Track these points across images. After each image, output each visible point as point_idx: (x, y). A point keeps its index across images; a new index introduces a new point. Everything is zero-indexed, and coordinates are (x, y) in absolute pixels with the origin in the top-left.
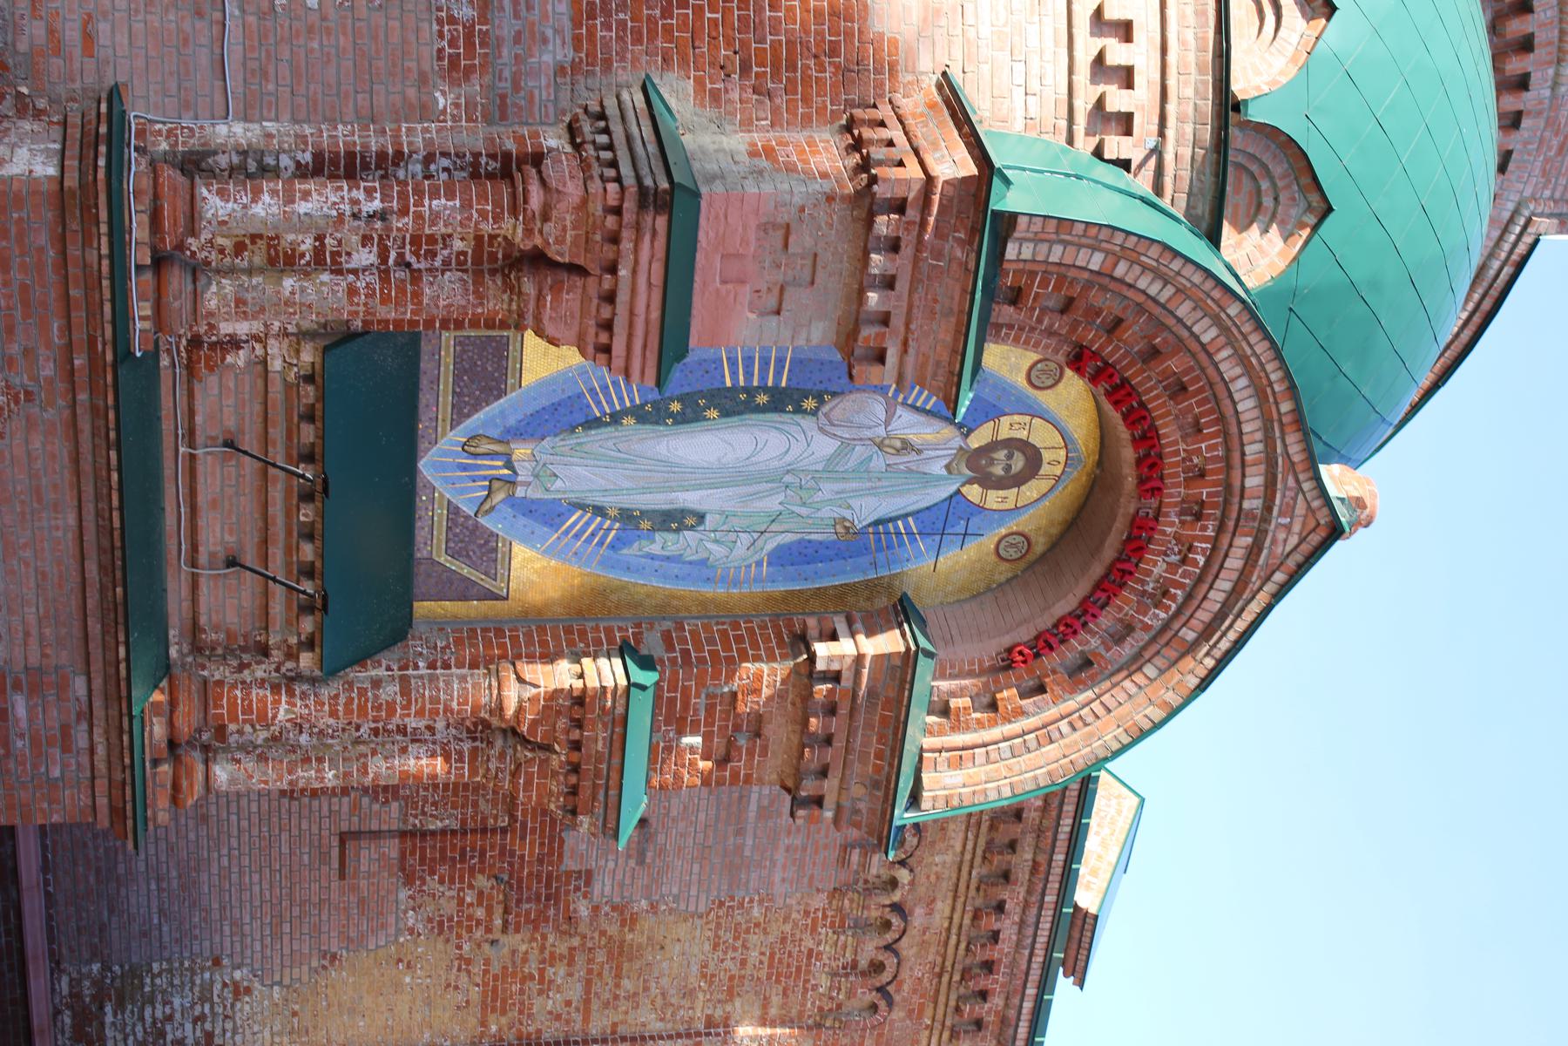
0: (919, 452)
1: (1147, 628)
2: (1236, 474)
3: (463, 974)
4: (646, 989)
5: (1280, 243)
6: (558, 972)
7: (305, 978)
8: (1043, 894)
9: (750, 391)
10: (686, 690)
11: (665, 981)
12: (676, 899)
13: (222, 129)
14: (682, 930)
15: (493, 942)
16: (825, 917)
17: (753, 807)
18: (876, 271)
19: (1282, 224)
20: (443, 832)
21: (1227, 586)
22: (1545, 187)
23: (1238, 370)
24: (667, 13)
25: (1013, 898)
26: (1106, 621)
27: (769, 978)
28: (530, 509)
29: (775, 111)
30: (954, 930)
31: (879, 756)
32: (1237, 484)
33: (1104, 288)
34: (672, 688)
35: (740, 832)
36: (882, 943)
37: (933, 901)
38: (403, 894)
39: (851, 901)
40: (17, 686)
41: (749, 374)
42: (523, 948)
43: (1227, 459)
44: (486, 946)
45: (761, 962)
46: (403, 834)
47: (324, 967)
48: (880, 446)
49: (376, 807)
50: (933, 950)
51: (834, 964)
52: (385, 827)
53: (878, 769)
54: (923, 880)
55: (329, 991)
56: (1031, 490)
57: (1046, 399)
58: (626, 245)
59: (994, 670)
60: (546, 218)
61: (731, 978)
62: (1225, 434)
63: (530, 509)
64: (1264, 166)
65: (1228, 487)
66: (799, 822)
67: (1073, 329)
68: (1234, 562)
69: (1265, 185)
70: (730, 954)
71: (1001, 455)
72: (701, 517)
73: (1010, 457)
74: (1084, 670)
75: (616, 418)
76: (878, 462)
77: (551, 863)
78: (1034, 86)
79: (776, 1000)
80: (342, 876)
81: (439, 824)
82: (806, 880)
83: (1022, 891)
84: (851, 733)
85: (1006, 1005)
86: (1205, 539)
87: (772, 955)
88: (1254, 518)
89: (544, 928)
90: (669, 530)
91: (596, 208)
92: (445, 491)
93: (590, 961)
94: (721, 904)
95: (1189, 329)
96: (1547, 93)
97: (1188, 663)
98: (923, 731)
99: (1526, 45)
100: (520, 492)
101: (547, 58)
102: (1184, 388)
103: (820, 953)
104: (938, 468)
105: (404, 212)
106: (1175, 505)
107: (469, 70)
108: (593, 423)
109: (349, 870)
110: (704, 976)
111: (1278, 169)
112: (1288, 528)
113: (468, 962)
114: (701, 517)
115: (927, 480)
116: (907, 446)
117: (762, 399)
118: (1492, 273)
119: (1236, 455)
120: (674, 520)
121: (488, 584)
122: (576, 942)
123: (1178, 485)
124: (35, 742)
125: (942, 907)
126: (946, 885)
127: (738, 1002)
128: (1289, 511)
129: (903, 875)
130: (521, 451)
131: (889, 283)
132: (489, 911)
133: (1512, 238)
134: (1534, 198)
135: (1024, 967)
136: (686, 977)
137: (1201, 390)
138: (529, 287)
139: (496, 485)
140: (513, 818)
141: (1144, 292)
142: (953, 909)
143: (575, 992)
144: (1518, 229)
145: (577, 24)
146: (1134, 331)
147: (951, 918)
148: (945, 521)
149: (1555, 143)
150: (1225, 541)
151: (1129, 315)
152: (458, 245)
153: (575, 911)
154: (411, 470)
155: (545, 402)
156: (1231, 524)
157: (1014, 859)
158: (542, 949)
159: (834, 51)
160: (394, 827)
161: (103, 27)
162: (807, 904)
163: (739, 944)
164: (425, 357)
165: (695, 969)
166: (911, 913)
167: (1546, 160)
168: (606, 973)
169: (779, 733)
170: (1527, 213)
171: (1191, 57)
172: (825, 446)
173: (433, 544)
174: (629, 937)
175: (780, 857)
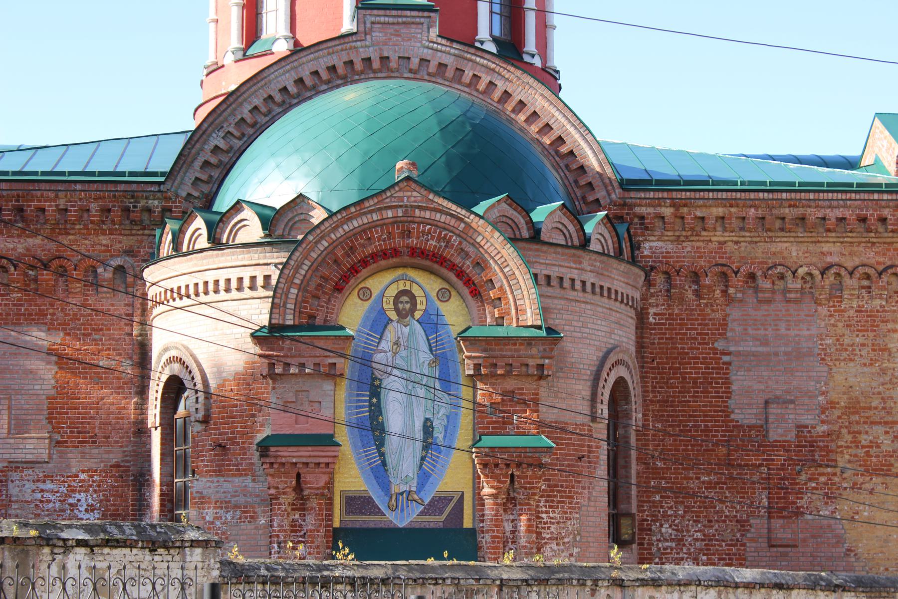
0: (399, 338)
1: (460, 243)
2: (386, 221)
3: (863, 486)
4: (879, 393)
5: (316, 211)
6: (864, 439)
7: (862, 564)
8: (810, 200)
9: (370, 406)
10: (488, 423)
11: (874, 384)
12: (818, 382)
14: (839, 378)
15: (842, 472)
16: (834, 306)
17: (760, 349)
18: (297, 371)
19: (310, 211)
20: (769, 498)
21: (438, 215)
22: (416, 38)
23: (340, 230)
24: (238, 444)
25: (813, 214)
26: (458, 260)
27: (875, 331)
28: (421, 485)
30: (841, 240)
31: (515, 344)
32: (391, 220)
33: (308, 285)
34: (488, 428)
35: (776, 354)
36: (848, 276)
37: (822, 253)
39: (820, 295)
41: (364, 407)
42: (847, 457)
43: (382, 225)
44: (845, 475)
45: (864, 336)
46: (770, 517)
47: (855, 555)
48: (396, 353)
49: (753, 530)
50: (855, 249)
51: (866, 298)
52: (766, 526)
53: (521, 344)
54: (808, 259)
55: (872, 552)
57: (375, 293)
58: (284, 460)
59: (482, 302)
60: (277, 488)
61: (874, 350)
62: (370, 229)
63: (421, 485)
64: (289, 220)
65: (393, 223)
66: (550, 373)
67: (326, 293)
68: (427, 214)
69: (297, 219)
70: (858, 352)
71: (401, 306)
72: (427, 420)
73: (402, 302)
74: (481, 264)
75: (382, 455)
76: (403, 353)
77: (790, 446)
78: (258, 311)
80: (795, 546)
81: (765, 500)
82: (809, 318)
83: (809, 210)
84: (503, 357)
85: (888, 207)
86: (419, 227)
87: (858, 330)
88: (406, 211)
89: (833, 446)
90: (432, 431)
91: (272, 471)
92: (414, 516)
93: (858, 423)
94: (823, 359)
95: (322, 252)
96: (371, 49)
97: (474, 225)
98: (510, 329)
99: (300, 81)
100: (414, 489)
101: (251, 485)
102: (351, 247)
103: (859, 306)
104: (406, 330)
105: (278, 536)
106: (404, 241)
107: (255, 512)
108: (384, 464)
109: (791, 543)
110: (871, 364)
111: (290, 215)
112: (409, 197)
113: (855, 484)
114: (427, 420)
115: (412, 333)
116: (397, 343)
118: (456, 52)
119: (378, 223)
120: (428, 428)
121: (455, 500)
122: (844, 431)
123: (394, 242)
125: (826, 248)
126: (812, 247)
127: (890, 345)
128: (401, 199)
129: (801, 271)
130: (395, 489)
131: (302, 366)
132: (823, 474)
133: (439, 47)
134: (421, 42)
135: (859, 202)
136: (873, 374)
137: (352, 241)
138: (306, 493)
139: (410, 498)
140: (761, 465)
141: (307, 272)
142: (827, 242)
143: (879, 430)
144: (435, 45)
145: (241, 475)
146: (325, 271)
147: (834, 242)
149: (395, 39)
150: (417, 220)
151: (319, 274)
152: (297, 516)
153: (824, 432)
154: (404, 529)
155: (374, 481)
156: (409, 219)
157: (789, 217)
158: (848, 447)
159: (248, 384)
160: (766, 521)
162: (825, 316)
163: (850, 349)
164: (354, 526)
165: (866, 369)
166: (829, 263)
167: (403, 40)
168: (866, 415)
169: (511, 384)
170: (427, 44)
171: (246, 256)
173: (437, 521)
174: (843, 404)
175: (793, 333)
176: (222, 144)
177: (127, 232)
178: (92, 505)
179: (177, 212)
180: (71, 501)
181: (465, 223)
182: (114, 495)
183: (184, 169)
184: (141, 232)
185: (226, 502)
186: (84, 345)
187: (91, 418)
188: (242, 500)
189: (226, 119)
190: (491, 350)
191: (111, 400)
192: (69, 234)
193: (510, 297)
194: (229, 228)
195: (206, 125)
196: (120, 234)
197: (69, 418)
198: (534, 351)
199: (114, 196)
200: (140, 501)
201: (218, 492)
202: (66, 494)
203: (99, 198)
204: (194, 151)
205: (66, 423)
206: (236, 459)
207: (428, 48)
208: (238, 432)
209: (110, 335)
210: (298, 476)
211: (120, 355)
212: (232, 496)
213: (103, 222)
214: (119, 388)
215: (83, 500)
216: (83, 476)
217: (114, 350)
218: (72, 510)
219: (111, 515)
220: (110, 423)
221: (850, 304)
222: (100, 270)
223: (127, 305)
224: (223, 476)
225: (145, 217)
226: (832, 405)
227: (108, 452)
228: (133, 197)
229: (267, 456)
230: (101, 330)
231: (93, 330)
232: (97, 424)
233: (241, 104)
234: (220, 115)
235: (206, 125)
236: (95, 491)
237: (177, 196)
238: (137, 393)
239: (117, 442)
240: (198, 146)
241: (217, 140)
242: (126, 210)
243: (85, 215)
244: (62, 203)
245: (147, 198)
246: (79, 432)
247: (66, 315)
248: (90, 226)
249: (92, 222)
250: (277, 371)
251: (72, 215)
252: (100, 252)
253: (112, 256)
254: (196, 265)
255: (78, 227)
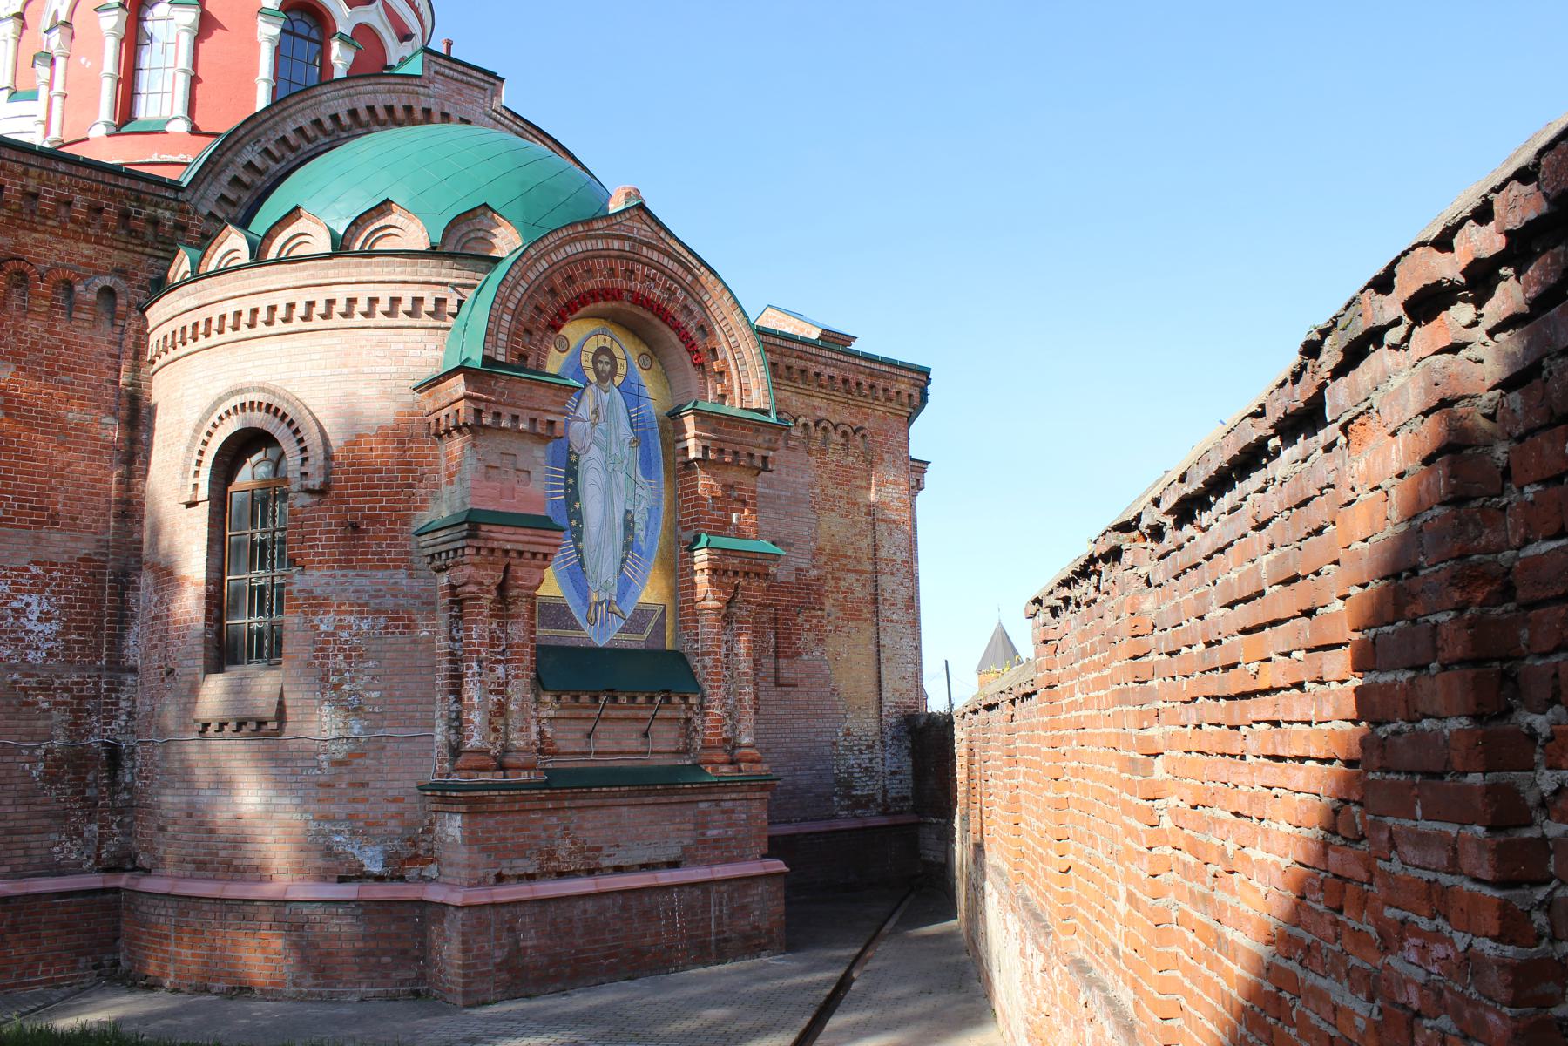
6: (843, 585)
9: (567, 487)
13: (438, 738)
14: (825, 526)
24: (383, 524)
25: (813, 368)
26: (682, 318)
28: (622, 594)
29: (431, 472)
35: (779, 497)
38: (805, 657)
40: (703, 834)
41: (559, 487)
46: (777, 657)
56: (618, 352)
57: (573, 344)
58: (495, 545)
59: (704, 372)
63: (622, 594)
65: (618, 257)
68: (655, 255)
72: (628, 512)
74: (705, 330)
75: (579, 552)
76: (603, 426)
79: (859, 482)
84: (732, 442)
91: (477, 559)
92: (613, 634)
97: (703, 280)
98: (733, 408)
99: (353, 113)
104: (606, 397)
105: (478, 652)
107: (410, 620)
108: (581, 563)
114: (628, 512)
115: (612, 401)
116: (595, 412)
117: (571, 481)
121: (658, 614)
124: (729, 825)
125: (817, 402)
126: (807, 400)
128: (631, 229)
129: (802, 420)
130: (594, 598)
131: (515, 418)
138: (515, 592)
143: (852, 577)
145: (388, 567)
146: (541, 300)
148: (631, 394)
151: (534, 302)
152: (494, 626)
154: (603, 650)
161: (390, 793)
169: (732, 476)
172: (594, 451)
173: (638, 640)
176: (258, 161)
177: (121, 245)
178: (48, 612)
179: (194, 234)
180: (15, 604)
181: (693, 275)
182: (81, 600)
183: (209, 179)
184: (140, 249)
185: (359, 605)
186: (46, 386)
187: (51, 489)
188: (389, 602)
189: (265, 133)
190: (720, 432)
191: (82, 467)
192: (36, 231)
193: (734, 372)
194: (365, 234)
195: (242, 132)
196: (111, 246)
197: (16, 486)
198: (760, 440)
199: (112, 192)
200: (121, 609)
201: (344, 590)
202: (8, 596)
203: (90, 190)
204: (224, 160)
205: (12, 493)
206: (380, 545)
207: (490, 117)
208: (382, 508)
209: (85, 379)
210: (507, 567)
211: (99, 407)
212: (371, 597)
213: (88, 225)
214: (95, 452)
215: (35, 605)
216: (34, 570)
217: (90, 400)
218: (17, 619)
219: (76, 628)
220: (80, 499)
221: (834, 457)
222: (79, 288)
223: (111, 342)
224: (354, 568)
225: (149, 230)
226: (820, 551)
227: (76, 540)
228: (138, 199)
229: (476, 537)
230: (73, 370)
231: (62, 368)
232: (60, 498)
233: (284, 119)
234: (260, 124)
235: (242, 132)
236: (53, 592)
237: (196, 212)
238: (121, 462)
239: (89, 527)
240: (229, 155)
241: (251, 154)
242: (125, 216)
243: (63, 210)
244: (32, 184)
245: (157, 205)
246: (32, 508)
247: (21, 341)
248: (70, 225)
249: (73, 220)
250: (485, 421)
251: (47, 202)
252: (80, 263)
253: (96, 273)
254: (313, 276)
255: (50, 222)
